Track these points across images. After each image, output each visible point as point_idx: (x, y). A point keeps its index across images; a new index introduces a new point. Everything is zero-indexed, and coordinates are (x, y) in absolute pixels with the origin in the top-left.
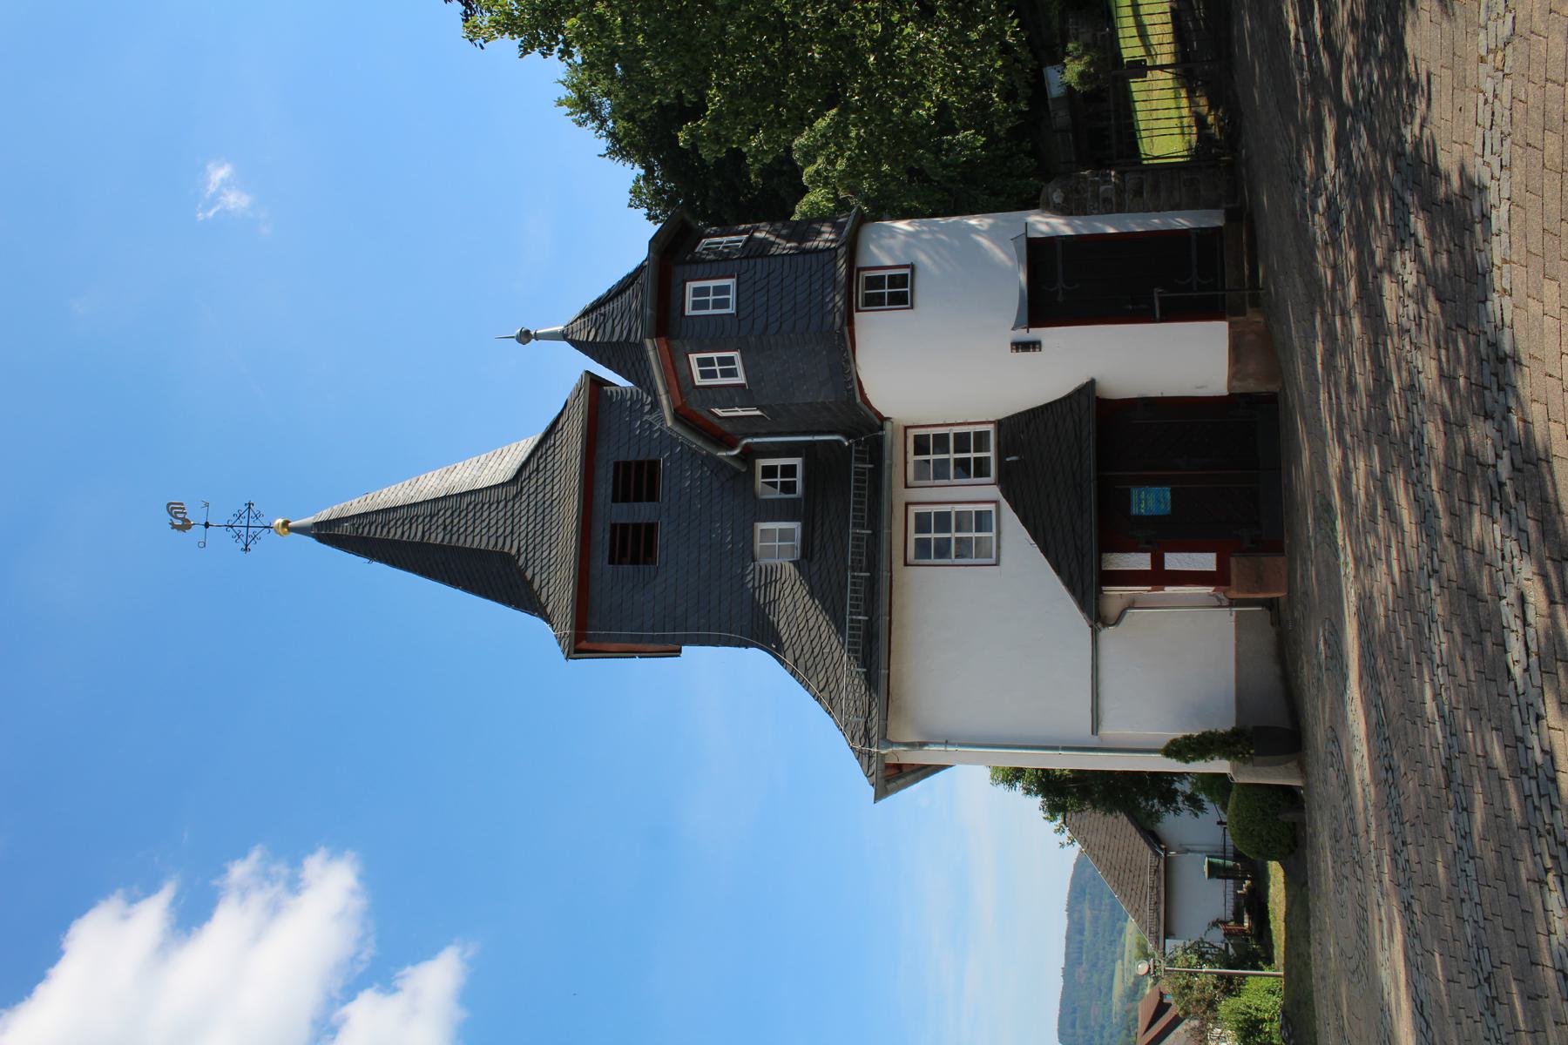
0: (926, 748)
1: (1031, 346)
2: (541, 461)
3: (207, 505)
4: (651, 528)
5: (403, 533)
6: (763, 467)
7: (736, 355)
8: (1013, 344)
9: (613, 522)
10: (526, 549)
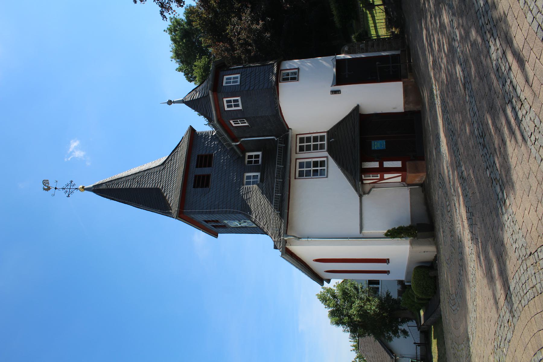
0: (300, 240)
2: (173, 157)
3: (57, 182)
4: (208, 176)
6: (248, 156)
7: (238, 98)
8: (331, 91)
9: (195, 174)
10: (165, 186)
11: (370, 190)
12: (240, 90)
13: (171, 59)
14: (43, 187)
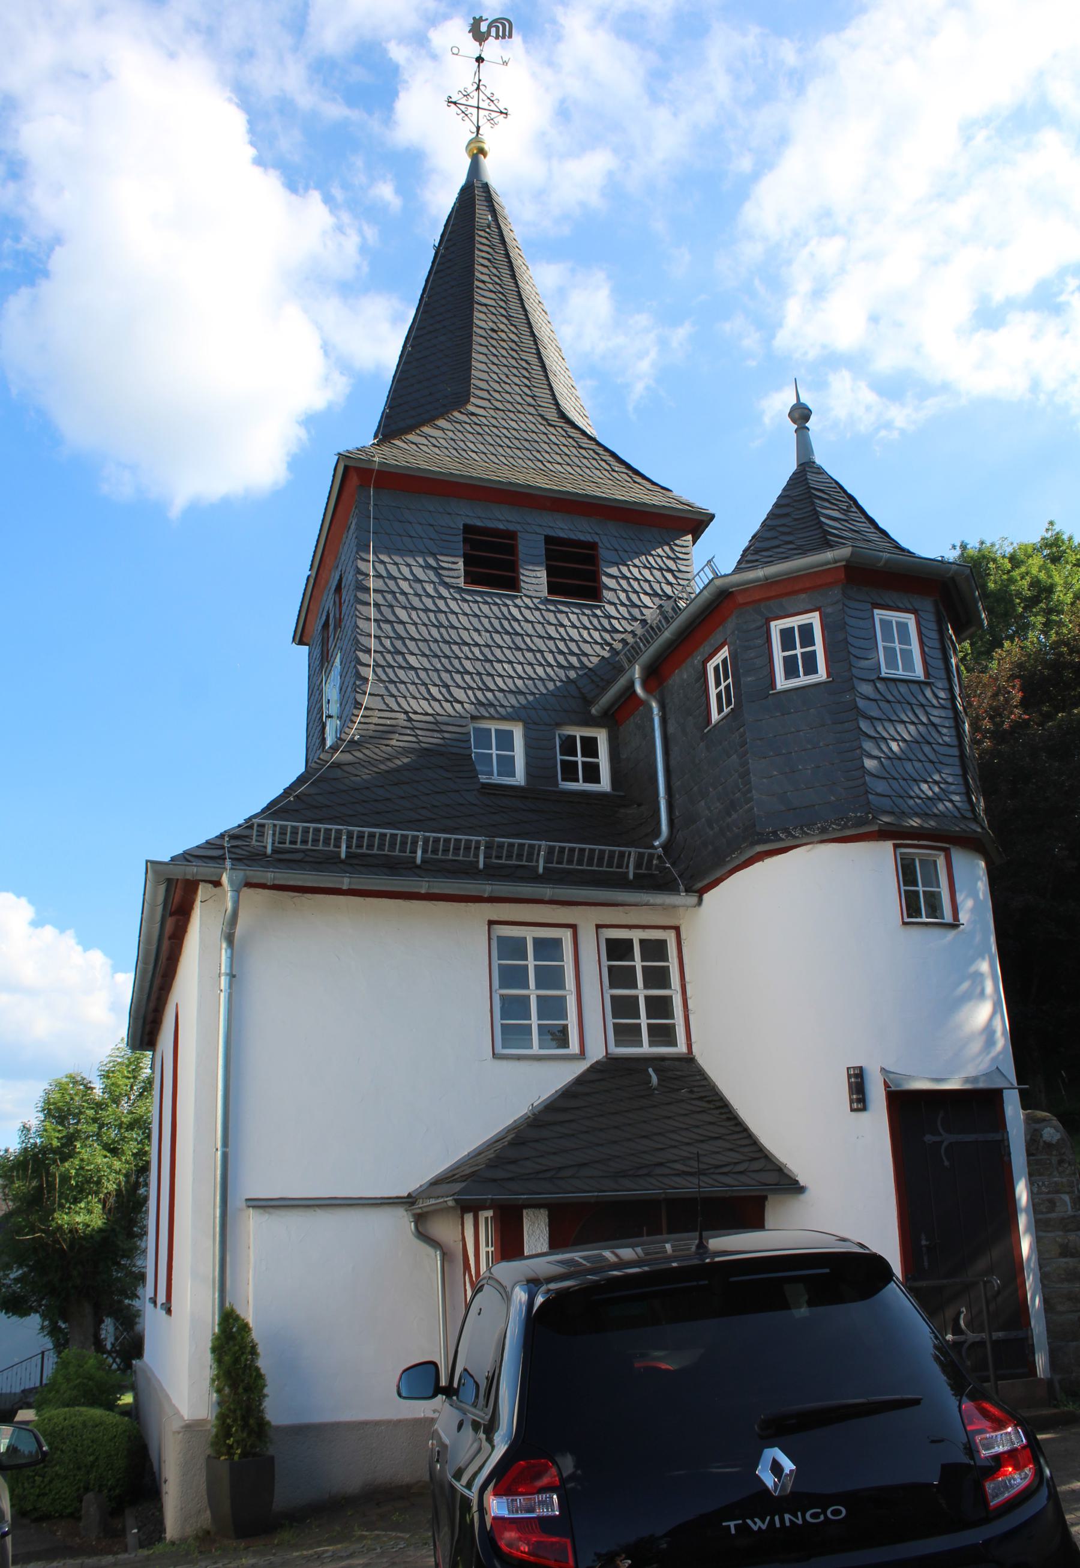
0: (224, 945)
2: (591, 452)
3: (505, 63)
5: (483, 282)
6: (596, 739)
7: (822, 674)
8: (861, 1068)
12: (855, 656)
13: (958, 544)
14: (487, 19)
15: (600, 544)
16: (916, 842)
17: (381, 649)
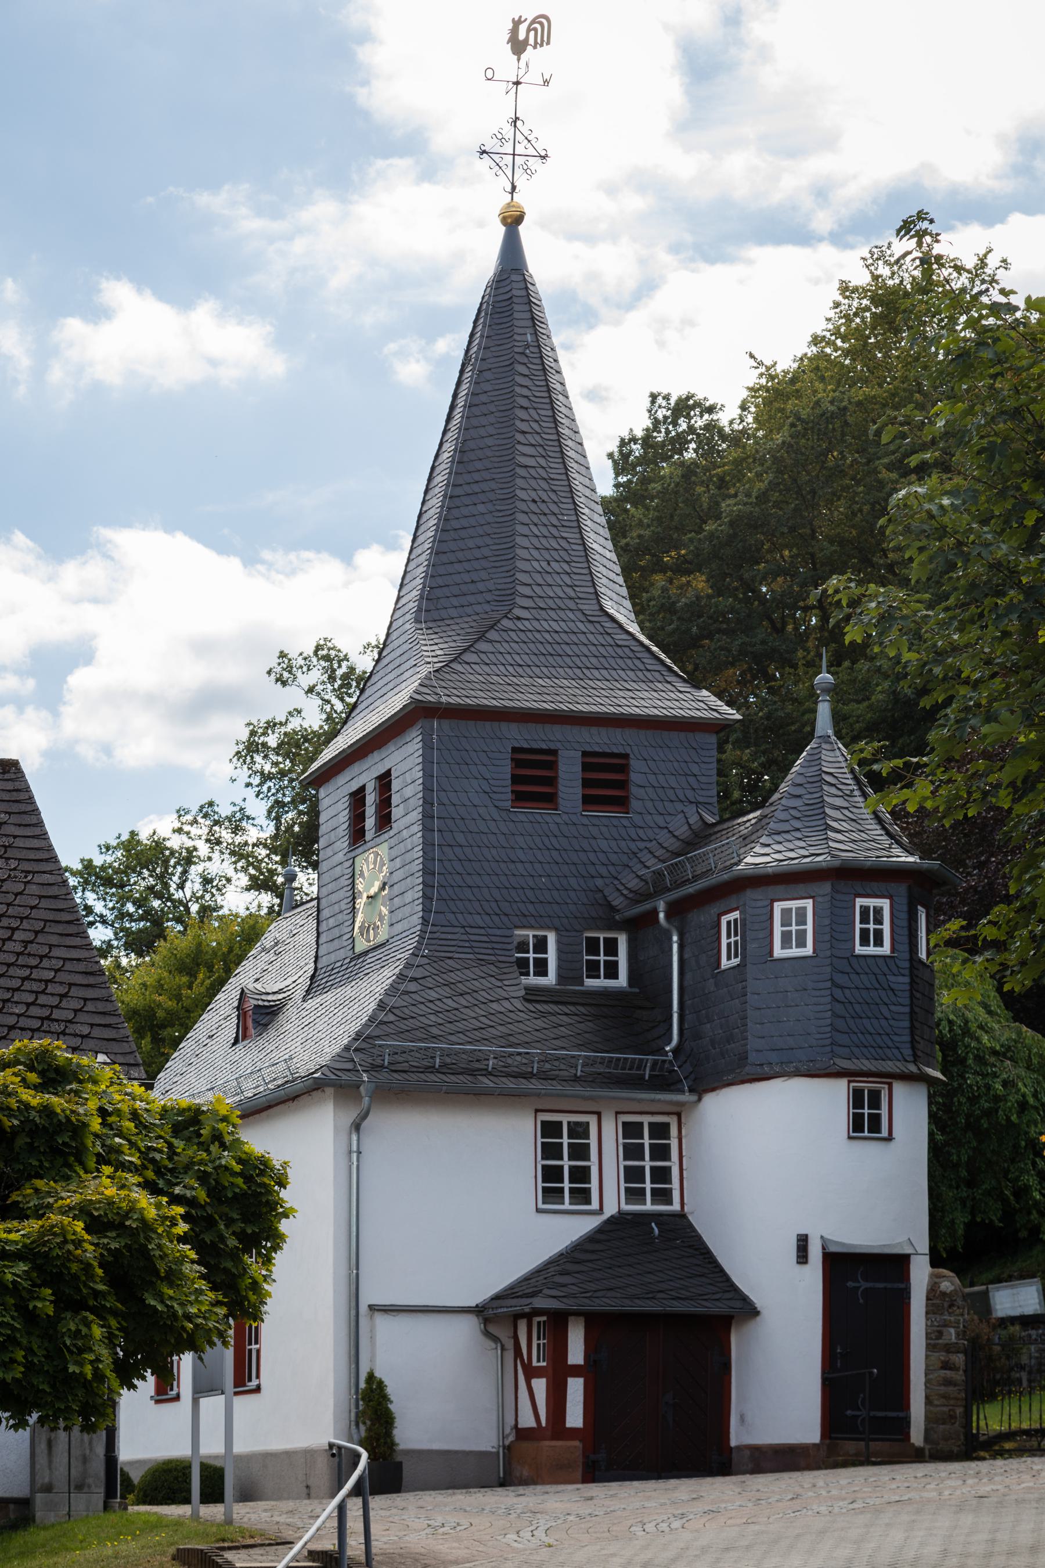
1: (802, 1254)
3: (546, 83)
4: (550, 799)
7: (808, 950)
8: (807, 1236)
11: (495, 1339)
15: (632, 756)
16: (865, 1079)
17: (444, 871)
